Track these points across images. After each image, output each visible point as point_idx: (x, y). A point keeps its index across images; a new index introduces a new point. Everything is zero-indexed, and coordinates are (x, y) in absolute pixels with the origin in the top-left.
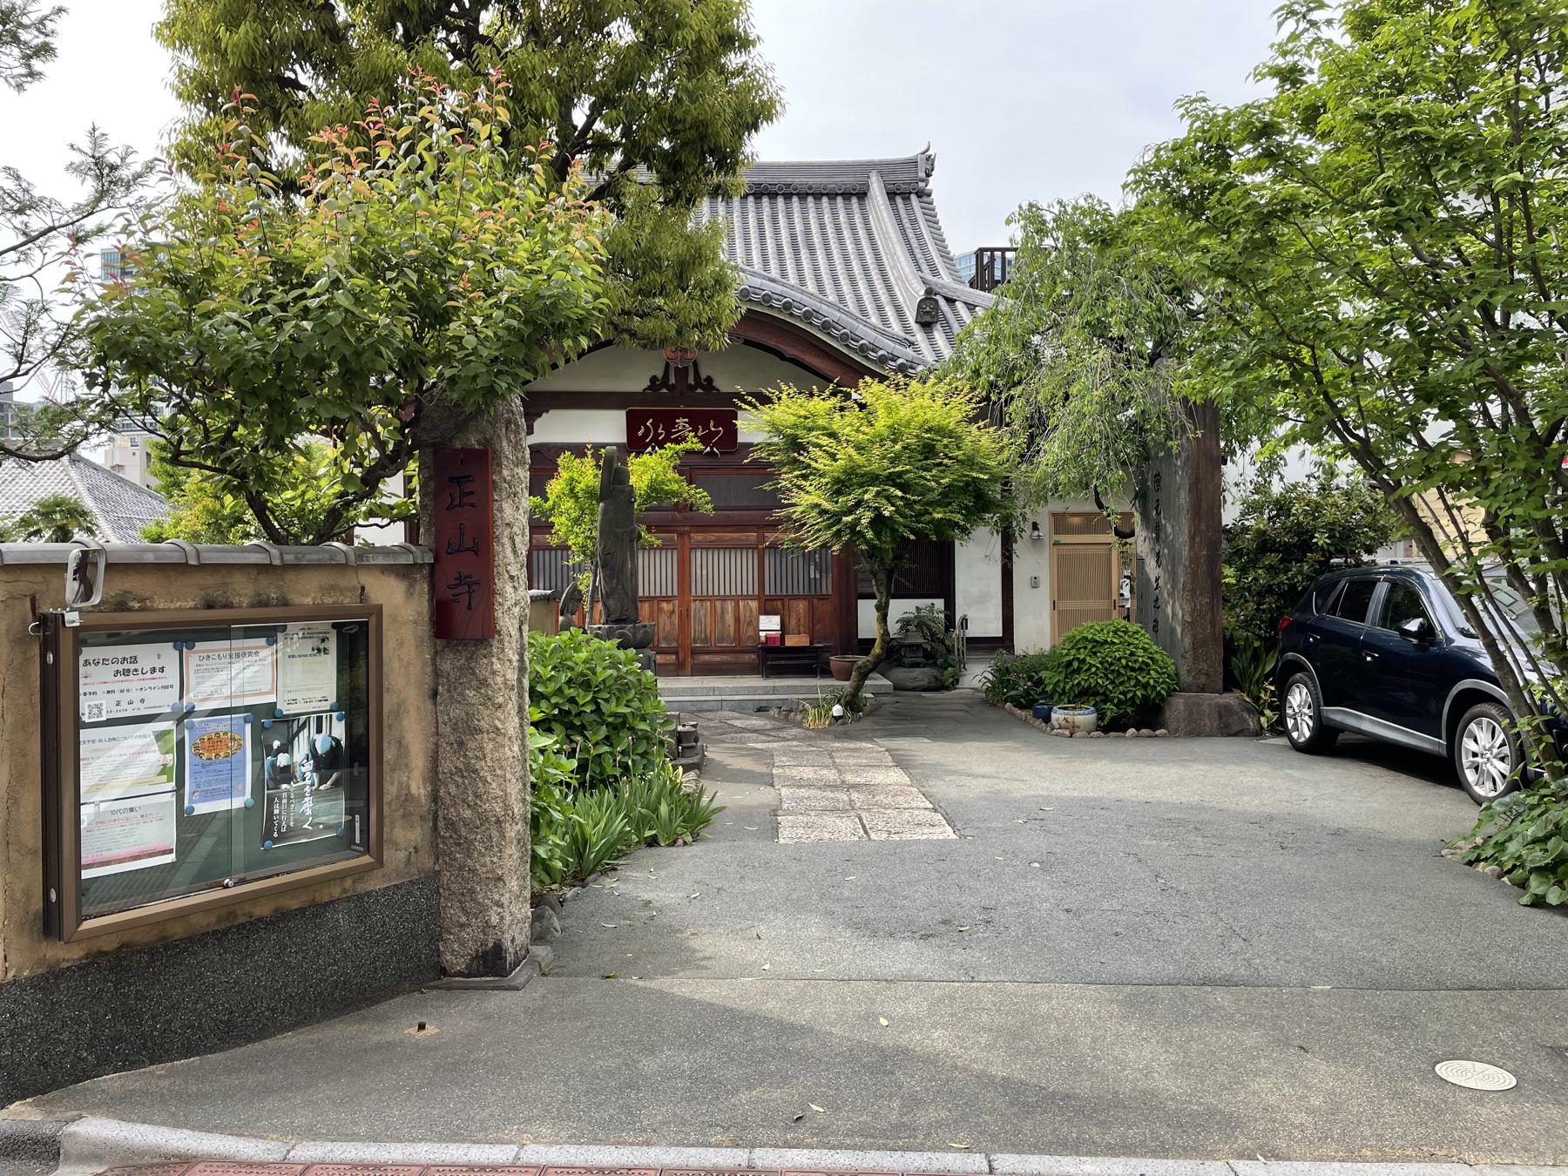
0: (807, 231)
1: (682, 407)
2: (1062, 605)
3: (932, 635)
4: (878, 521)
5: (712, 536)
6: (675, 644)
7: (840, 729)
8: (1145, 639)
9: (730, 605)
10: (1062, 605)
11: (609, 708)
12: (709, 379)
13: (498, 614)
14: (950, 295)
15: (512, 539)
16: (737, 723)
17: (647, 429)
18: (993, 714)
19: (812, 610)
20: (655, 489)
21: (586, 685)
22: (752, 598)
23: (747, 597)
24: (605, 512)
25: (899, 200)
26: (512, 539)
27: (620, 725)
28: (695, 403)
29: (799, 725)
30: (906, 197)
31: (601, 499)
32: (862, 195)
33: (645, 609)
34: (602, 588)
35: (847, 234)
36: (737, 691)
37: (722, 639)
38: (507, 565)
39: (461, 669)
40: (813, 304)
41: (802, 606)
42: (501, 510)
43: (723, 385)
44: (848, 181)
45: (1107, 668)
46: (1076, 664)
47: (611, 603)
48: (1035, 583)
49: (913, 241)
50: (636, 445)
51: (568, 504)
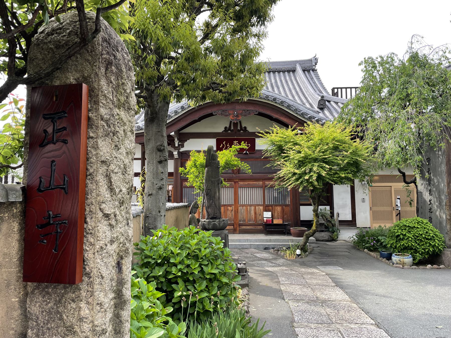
0: (276, 82)
1: (236, 137)
2: (375, 209)
3: (327, 219)
4: (320, 177)
5: (246, 183)
6: (233, 222)
7: (300, 260)
8: (430, 226)
9: (253, 208)
10: (375, 209)
11: (208, 270)
12: (245, 128)
13: (88, 255)
14: (328, 99)
15: (108, 177)
16: (258, 255)
17: (223, 145)
18: (359, 254)
19: (283, 210)
20: (228, 164)
21: (196, 257)
22: (261, 205)
23: (259, 205)
24: (208, 172)
25: (306, 72)
26: (108, 177)
27: (213, 279)
28: (240, 135)
29: (283, 257)
30: (309, 71)
31: (207, 166)
32: (294, 71)
33: (222, 209)
34: (206, 204)
35: (289, 83)
36: (256, 241)
37: (250, 221)
38: (100, 203)
39: (50, 313)
40: (284, 99)
41: (279, 209)
42: (96, 147)
43: (250, 129)
44: (290, 67)
45: (416, 238)
46: (401, 237)
47: (209, 210)
48: (363, 200)
49: (313, 84)
50: (219, 149)
51: (194, 169)
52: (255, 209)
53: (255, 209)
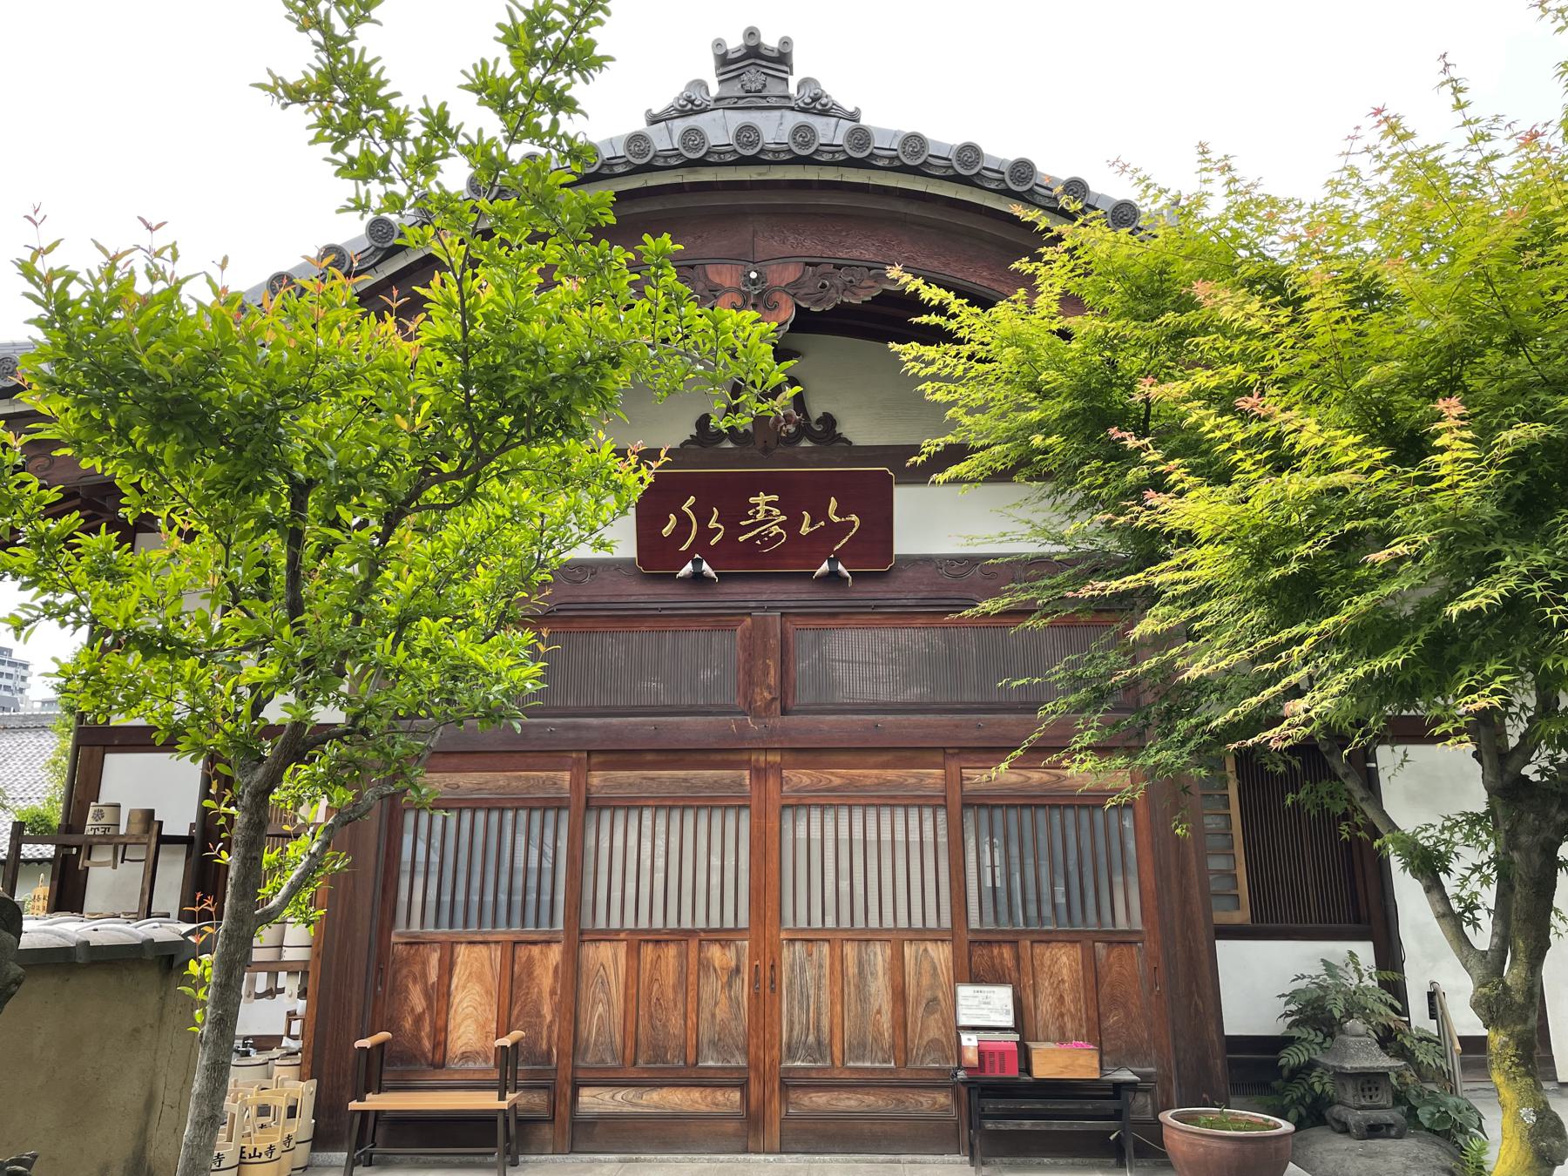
9: (880, 955)
37: (860, 1049)
52: (898, 957)
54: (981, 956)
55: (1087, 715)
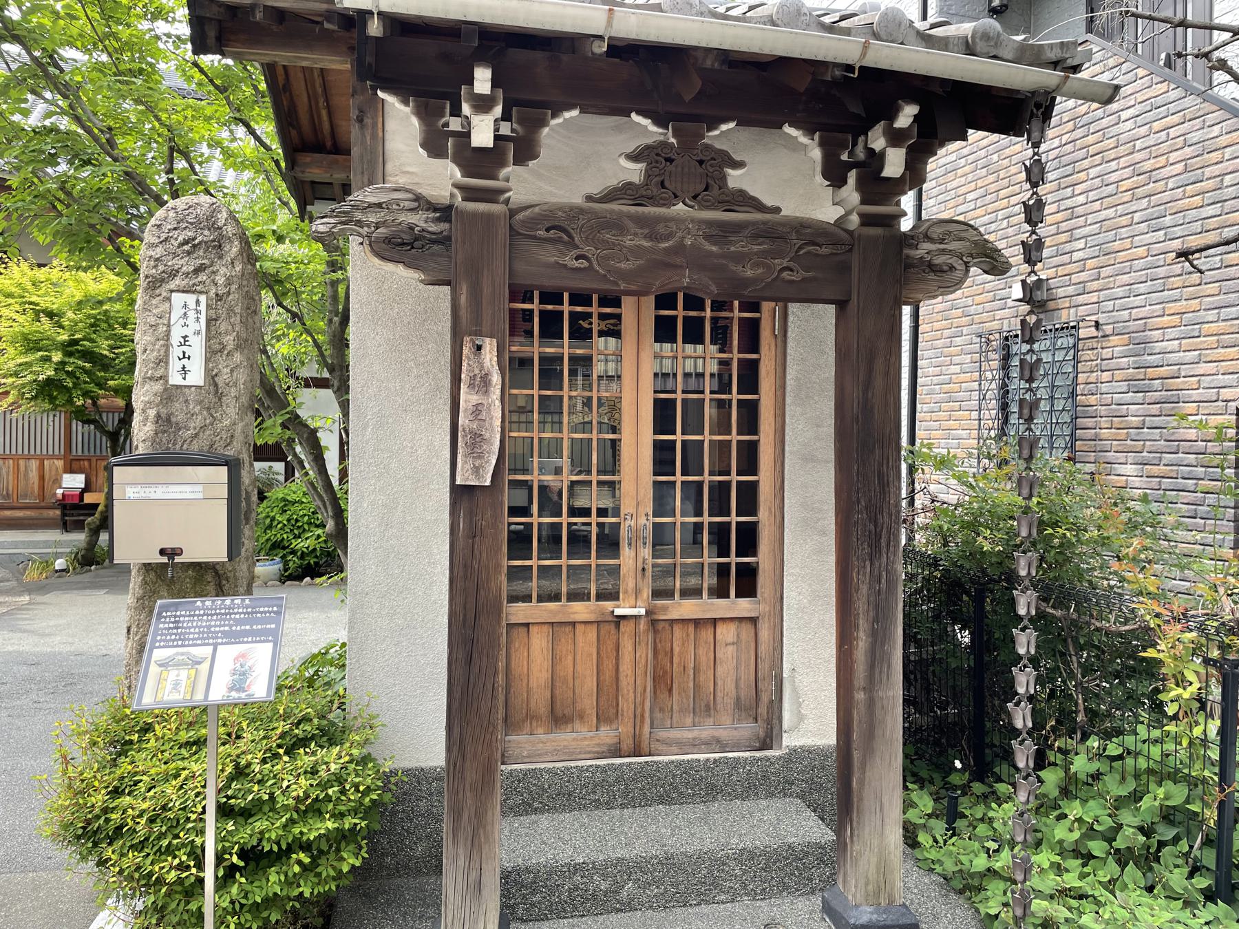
9: (34, 464)
37: (25, 496)
52: (42, 466)
53: (42, 466)
54: (75, 465)
55: (1067, 438)
